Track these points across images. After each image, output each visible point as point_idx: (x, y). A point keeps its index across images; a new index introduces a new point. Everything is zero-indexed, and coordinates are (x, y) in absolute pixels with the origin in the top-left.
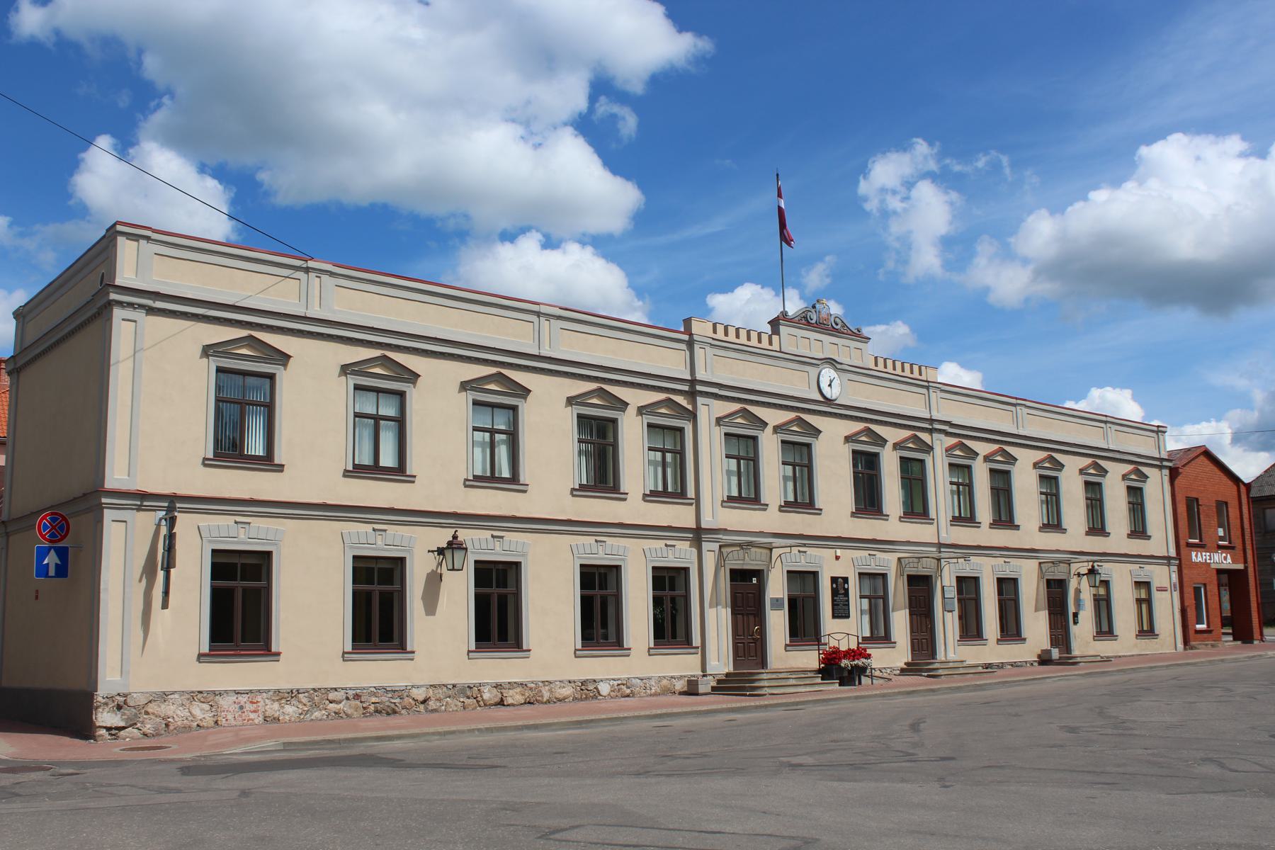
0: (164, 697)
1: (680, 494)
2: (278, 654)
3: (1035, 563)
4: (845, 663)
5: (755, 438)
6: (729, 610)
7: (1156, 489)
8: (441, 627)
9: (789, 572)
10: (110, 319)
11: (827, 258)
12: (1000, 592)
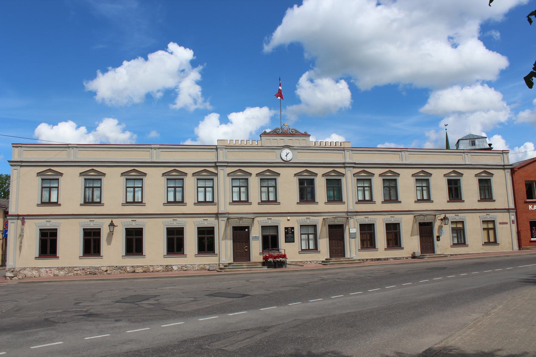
0: (25, 269)
3: (411, 217)
6: (328, 239)
8: (113, 250)
9: (262, 226)
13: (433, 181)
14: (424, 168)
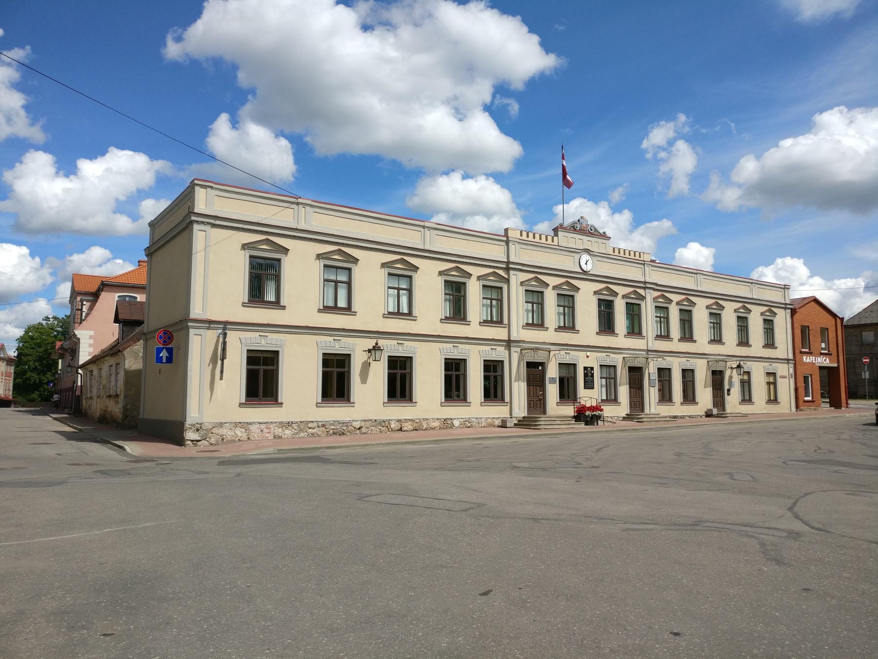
0: (221, 425)
1: (500, 322)
2: (282, 404)
3: (705, 362)
4: (588, 413)
5: (542, 293)
7: (782, 322)
8: (369, 389)
10: (192, 230)
11: (625, 185)
12: (684, 377)
13: (579, 298)
14: (610, 283)
